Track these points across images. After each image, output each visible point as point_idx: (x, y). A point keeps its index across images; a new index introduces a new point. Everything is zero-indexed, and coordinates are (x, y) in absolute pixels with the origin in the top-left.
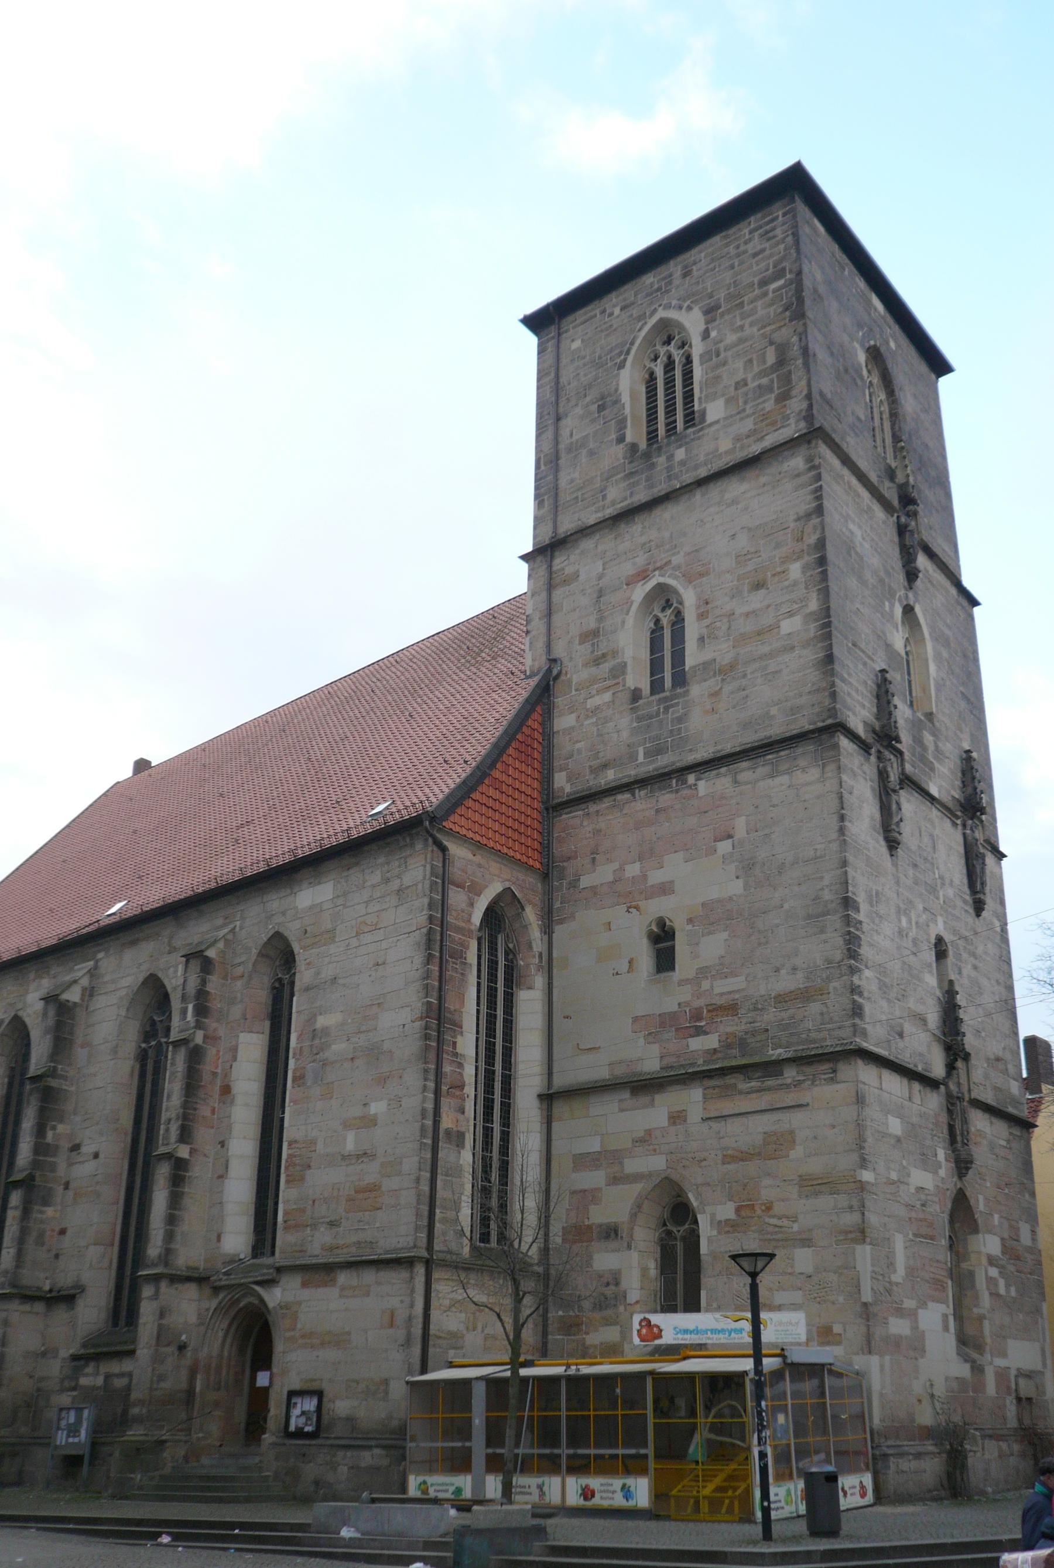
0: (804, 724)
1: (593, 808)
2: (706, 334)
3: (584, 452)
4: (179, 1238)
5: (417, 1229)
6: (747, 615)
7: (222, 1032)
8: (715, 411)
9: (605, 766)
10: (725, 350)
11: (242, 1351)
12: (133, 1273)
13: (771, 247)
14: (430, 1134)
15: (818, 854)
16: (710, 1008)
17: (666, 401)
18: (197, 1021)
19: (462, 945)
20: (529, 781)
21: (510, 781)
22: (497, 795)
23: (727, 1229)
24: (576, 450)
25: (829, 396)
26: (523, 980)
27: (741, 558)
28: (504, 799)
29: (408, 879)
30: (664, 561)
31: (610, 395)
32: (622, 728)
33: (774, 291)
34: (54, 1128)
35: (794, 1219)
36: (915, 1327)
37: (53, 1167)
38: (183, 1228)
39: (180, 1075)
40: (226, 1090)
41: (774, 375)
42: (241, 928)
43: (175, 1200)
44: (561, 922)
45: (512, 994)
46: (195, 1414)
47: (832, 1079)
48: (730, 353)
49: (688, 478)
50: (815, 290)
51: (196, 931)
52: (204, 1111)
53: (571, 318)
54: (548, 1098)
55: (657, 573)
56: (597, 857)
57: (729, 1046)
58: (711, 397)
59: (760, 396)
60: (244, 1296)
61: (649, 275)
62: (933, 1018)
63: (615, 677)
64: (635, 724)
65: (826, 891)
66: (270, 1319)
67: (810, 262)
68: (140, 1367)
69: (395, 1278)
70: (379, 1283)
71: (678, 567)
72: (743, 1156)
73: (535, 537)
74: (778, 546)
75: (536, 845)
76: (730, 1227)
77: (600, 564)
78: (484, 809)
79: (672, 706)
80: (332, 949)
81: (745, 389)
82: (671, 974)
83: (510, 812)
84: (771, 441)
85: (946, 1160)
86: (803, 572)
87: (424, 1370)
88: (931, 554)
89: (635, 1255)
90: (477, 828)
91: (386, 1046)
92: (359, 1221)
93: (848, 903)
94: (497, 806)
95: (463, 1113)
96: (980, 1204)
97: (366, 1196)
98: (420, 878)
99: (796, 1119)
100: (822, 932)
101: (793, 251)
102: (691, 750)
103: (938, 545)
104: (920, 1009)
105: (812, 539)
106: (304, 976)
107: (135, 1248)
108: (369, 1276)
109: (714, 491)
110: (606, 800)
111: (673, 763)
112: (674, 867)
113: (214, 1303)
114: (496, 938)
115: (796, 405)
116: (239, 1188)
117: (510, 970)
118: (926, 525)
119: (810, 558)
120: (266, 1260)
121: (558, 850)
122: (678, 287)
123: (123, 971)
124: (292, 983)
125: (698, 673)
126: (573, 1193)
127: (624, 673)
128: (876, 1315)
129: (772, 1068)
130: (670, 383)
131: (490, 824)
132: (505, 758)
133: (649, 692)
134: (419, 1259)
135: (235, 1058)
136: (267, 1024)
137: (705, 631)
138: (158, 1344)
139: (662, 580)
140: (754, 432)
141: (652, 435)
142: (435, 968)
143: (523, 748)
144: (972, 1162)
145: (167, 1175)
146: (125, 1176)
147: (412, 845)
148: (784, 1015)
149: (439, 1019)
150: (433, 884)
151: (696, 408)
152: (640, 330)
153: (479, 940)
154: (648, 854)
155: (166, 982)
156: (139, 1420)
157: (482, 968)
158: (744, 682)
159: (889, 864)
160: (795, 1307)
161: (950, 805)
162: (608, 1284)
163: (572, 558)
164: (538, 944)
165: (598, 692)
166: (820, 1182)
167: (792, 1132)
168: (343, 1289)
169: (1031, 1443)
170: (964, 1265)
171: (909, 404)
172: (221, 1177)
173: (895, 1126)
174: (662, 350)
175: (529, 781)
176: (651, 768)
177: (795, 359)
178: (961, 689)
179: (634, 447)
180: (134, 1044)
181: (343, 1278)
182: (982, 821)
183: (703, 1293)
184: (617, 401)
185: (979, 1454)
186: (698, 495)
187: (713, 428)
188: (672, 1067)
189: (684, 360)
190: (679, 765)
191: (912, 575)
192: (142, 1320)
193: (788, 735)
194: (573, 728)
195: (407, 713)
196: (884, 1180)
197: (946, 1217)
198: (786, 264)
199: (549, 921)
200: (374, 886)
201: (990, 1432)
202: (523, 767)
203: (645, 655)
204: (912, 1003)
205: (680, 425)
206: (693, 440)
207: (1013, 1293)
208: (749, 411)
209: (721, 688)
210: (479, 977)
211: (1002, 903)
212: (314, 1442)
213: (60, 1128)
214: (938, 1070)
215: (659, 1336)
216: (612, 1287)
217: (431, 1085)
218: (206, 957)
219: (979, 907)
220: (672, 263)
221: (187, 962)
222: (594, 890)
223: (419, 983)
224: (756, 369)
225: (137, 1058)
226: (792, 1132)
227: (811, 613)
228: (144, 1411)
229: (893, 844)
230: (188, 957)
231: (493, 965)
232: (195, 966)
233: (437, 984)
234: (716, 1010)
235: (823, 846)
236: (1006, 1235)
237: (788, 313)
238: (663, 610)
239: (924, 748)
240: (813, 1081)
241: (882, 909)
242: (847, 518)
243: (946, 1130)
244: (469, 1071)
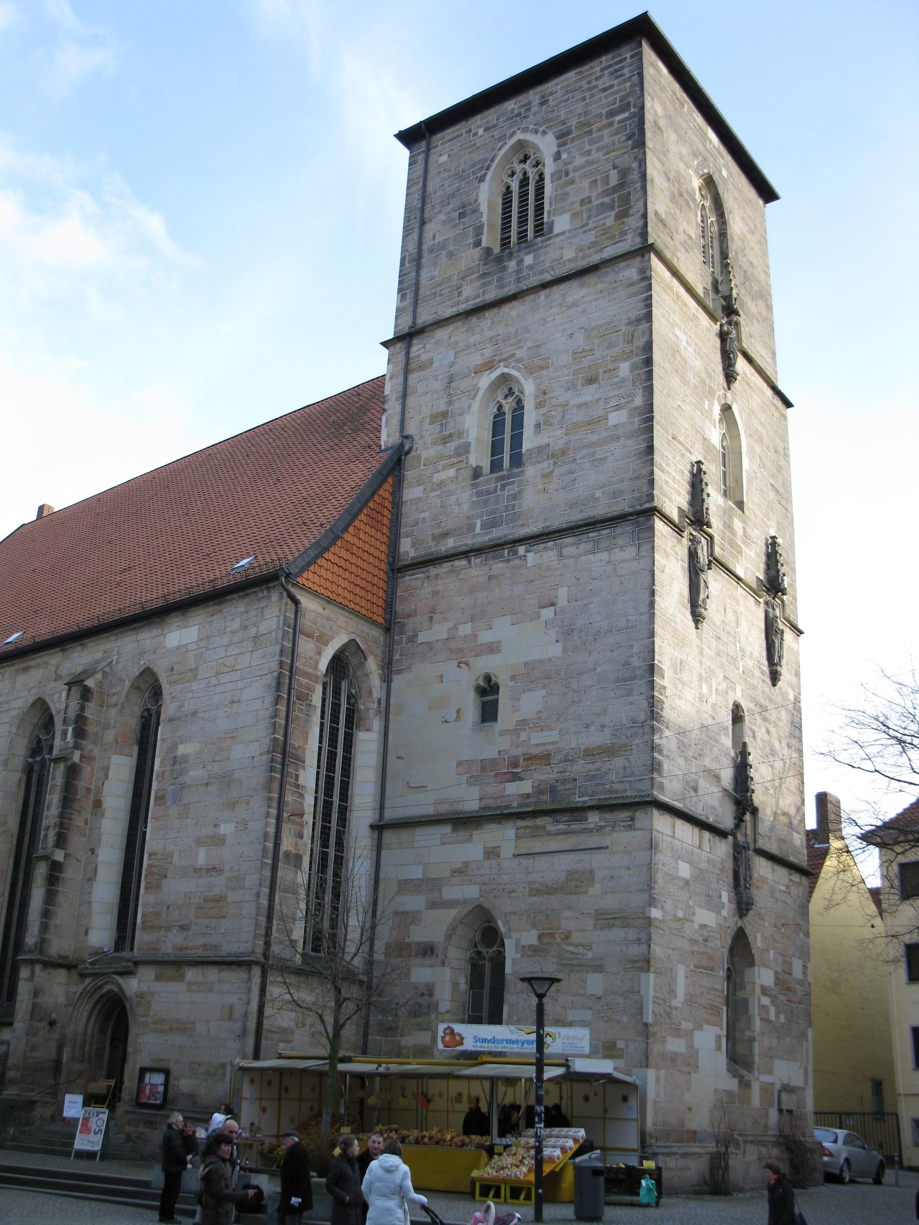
0: (623, 506)
1: (433, 571)
2: (557, 157)
3: (444, 253)
4: (52, 930)
5: (256, 937)
6: (579, 406)
7: (96, 753)
8: (561, 223)
9: (446, 535)
10: (574, 171)
11: (103, 1031)
12: (14, 957)
13: (619, 84)
14: (270, 854)
15: (630, 625)
16: (526, 757)
17: (520, 212)
18: (75, 742)
19: (308, 689)
20: (378, 545)
21: (361, 544)
23: (530, 953)
24: (438, 251)
25: (664, 216)
26: (362, 722)
27: (578, 355)
29: (263, 628)
30: (509, 354)
31: (470, 204)
32: (462, 502)
33: (619, 122)
35: (589, 947)
36: (690, 1046)
38: (56, 921)
39: (58, 789)
40: (98, 804)
41: (615, 195)
42: (117, 663)
43: (51, 896)
44: (399, 672)
45: (352, 734)
47: (630, 826)
48: (577, 174)
49: (534, 281)
50: (656, 123)
51: (79, 659)
52: (78, 821)
53: (440, 135)
54: (379, 828)
55: (502, 364)
56: (435, 616)
57: (541, 792)
58: (560, 211)
59: (602, 213)
60: (107, 983)
61: (510, 102)
62: (727, 775)
63: (459, 455)
64: (475, 499)
65: (635, 658)
66: (128, 1006)
67: (653, 100)
69: (236, 977)
70: (220, 982)
72: (549, 890)
73: (396, 326)
75: (381, 603)
76: (533, 951)
77: (451, 354)
78: (336, 569)
79: (509, 484)
80: (195, 686)
81: (589, 206)
82: (493, 724)
83: (359, 572)
84: (610, 253)
85: (729, 901)
86: (631, 371)
87: (256, 1057)
89: (447, 971)
90: (329, 585)
91: (237, 775)
92: (207, 927)
94: (348, 566)
95: (302, 838)
96: (757, 941)
97: (213, 904)
98: (275, 627)
99: (597, 860)
100: (629, 694)
101: (637, 89)
102: (523, 525)
104: (714, 766)
105: (641, 342)
106: (169, 708)
107: (16, 935)
108: (212, 973)
109: (557, 291)
110: (445, 565)
111: (506, 536)
112: (501, 629)
113: (81, 988)
114: (340, 684)
115: (633, 222)
117: (351, 713)
118: (750, 334)
119: (639, 359)
120: (125, 954)
121: (400, 608)
122: (535, 114)
124: (159, 714)
125: (533, 455)
126: (396, 913)
127: (468, 452)
128: (655, 1034)
129: (577, 812)
130: (524, 196)
131: (341, 582)
132: (357, 523)
133: (489, 470)
134: (257, 963)
135: (106, 777)
136: (136, 749)
137: (542, 418)
138: (32, 1018)
139: (506, 370)
141: (505, 242)
142: (282, 708)
143: (374, 515)
144: (752, 904)
145: (45, 874)
147: (269, 597)
148: (591, 767)
149: (284, 754)
150: (285, 633)
151: (545, 220)
152: (500, 149)
153: (325, 686)
154: (478, 616)
155: (51, 706)
156: (12, 1082)
157: (326, 710)
158: (574, 466)
159: (694, 637)
160: (583, 1024)
161: (754, 585)
162: (423, 995)
164: (378, 691)
165: (444, 468)
166: (613, 916)
167: (592, 871)
168: (189, 984)
169: (789, 1149)
170: (740, 994)
172: (90, 879)
173: (684, 870)
174: (518, 168)
175: (378, 545)
176: (486, 538)
177: (634, 183)
178: (771, 481)
179: (488, 251)
180: (22, 758)
181: (191, 974)
182: (783, 601)
183: (506, 1008)
184: (475, 211)
185: (740, 1156)
187: (559, 239)
188: (489, 808)
189: (537, 178)
191: (730, 377)
192: (19, 997)
193: (609, 515)
194: (419, 499)
195: (275, 477)
196: (671, 917)
197: (726, 951)
198: (631, 99)
199: (388, 670)
200: (233, 632)
201: (751, 1138)
202: (373, 532)
203: (487, 437)
204: (707, 762)
205: (530, 234)
206: (541, 248)
207: (782, 1019)
208: (591, 226)
209: (553, 471)
210: (322, 717)
212: (159, 1113)
214: (727, 822)
215: (461, 1044)
216: (426, 997)
217: (274, 812)
218: (86, 686)
219: (775, 677)
220: (531, 92)
221: (69, 690)
222: (429, 644)
223: (267, 721)
224: (600, 189)
225: (24, 771)
226: (592, 871)
227: (636, 408)
228: (19, 1074)
229: (697, 617)
230: (70, 684)
231: (336, 708)
232: (76, 691)
233: (283, 722)
235: (634, 618)
236: (779, 969)
237: (630, 142)
238: (506, 397)
239: (733, 533)
240: (613, 827)
241: (685, 677)
242: (673, 325)
243: (731, 876)
244: (309, 801)
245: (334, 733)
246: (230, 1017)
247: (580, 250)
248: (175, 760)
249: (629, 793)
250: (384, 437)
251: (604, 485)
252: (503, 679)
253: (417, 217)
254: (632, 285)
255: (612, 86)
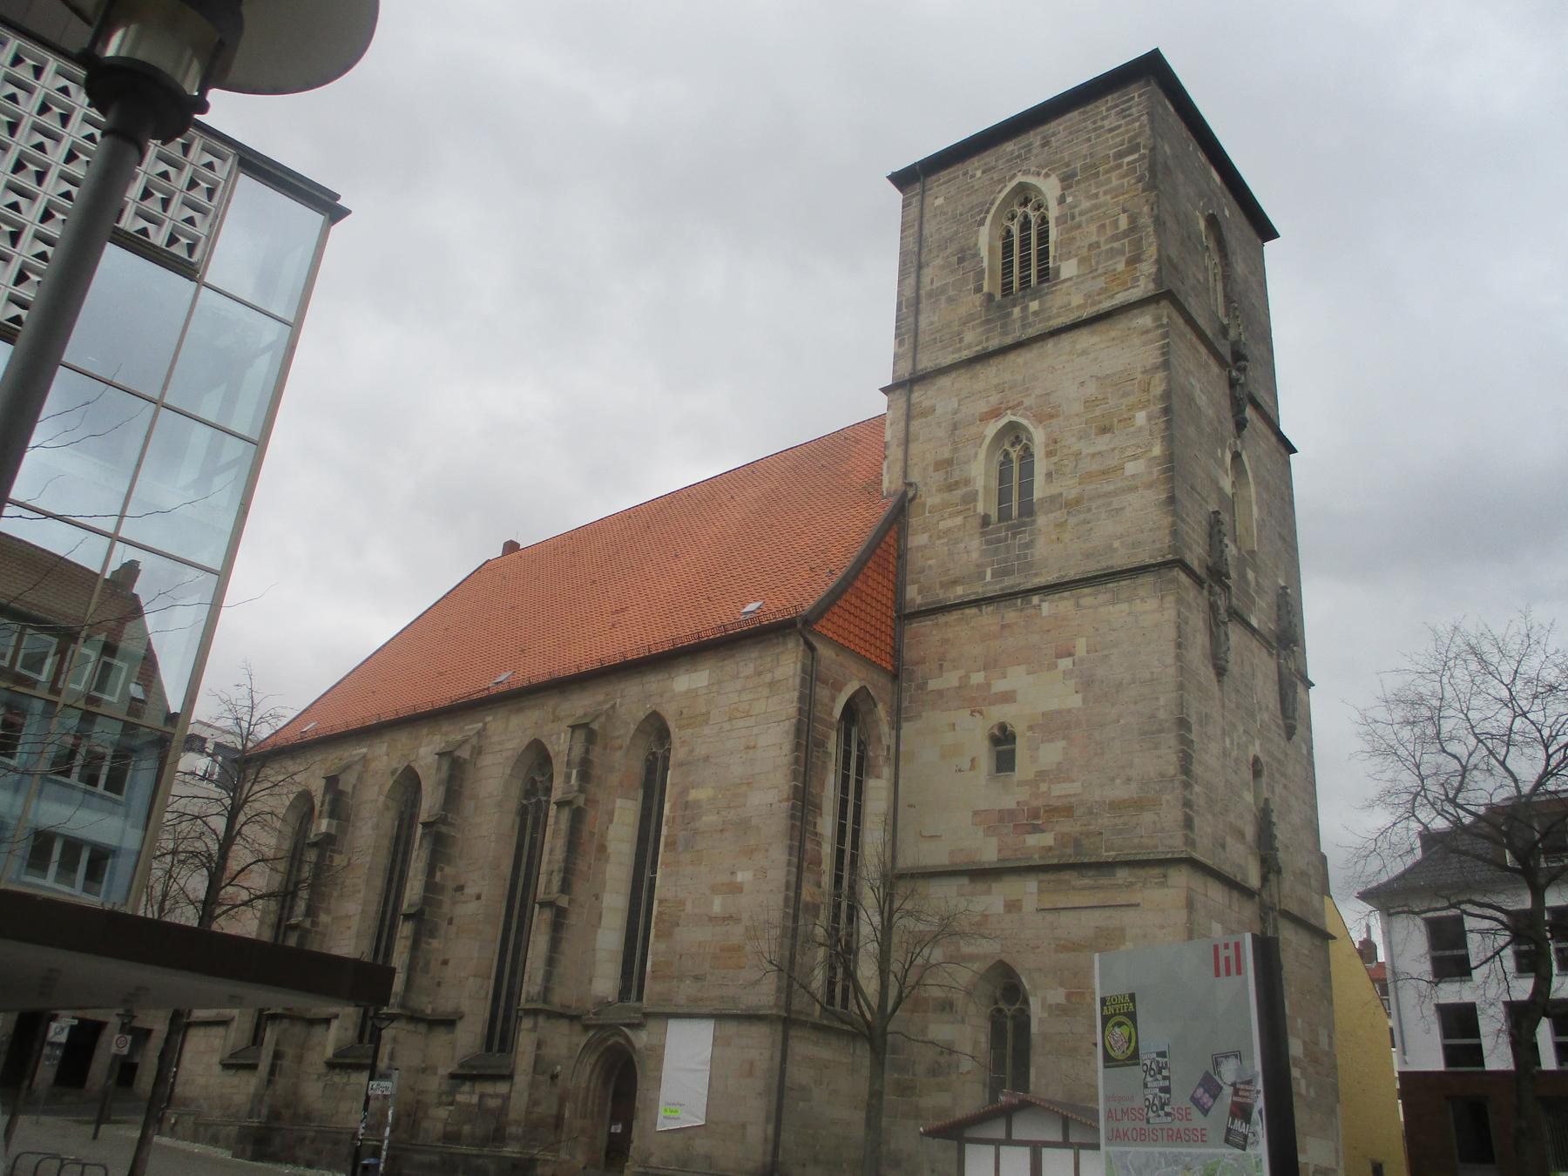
1: (942, 619)
3: (943, 298)
6: (1093, 455)
8: (1068, 269)
9: (955, 582)
13: (1127, 124)
22: (857, 602)
27: (1090, 403)
28: (863, 606)
29: (779, 673)
32: (972, 548)
34: (442, 870)
37: (439, 904)
40: (602, 848)
44: (908, 719)
46: (564, 1137)
51: (580, 705)
53: (934, 178)
62: (1250, 831)
66: (635, 1058)
68: (519, 1094)
71: (1029, 408)
74: (1125, 395)
76: (1060, 1011)
77: (955, 400)
80: (706, 730)
88: (1257, 406)
93: (1183, 723)
94: (858, 613)
99: (1128, 917)
100: (1156, 748)
103: (1262, 396)
106: (678, 753)
109: (1066, 341)
112: (1016, 679)
113: (583, 1040)
116: (609, 938)
117: (860, 760)
123: (508, 735)
124: (666, 759)
127: (975, 500)
129: (1105, 867)
130: (1025, 242)
135: (611, 821)
136: (641, 793)
138: (535, 1071)
139: (1014, 418)
140: (1103, 291)
141: (1007, 288)
146: (502, 919)
155: (549, 748)
158: (1089, 516)
163: (930, 393)
165: (951, 516)
171: (1240, 268)
174: (1019, 211)
183: (1033, 1071)
184: (976, 255)
186: (1050, 345)
190: (1022, 587)
191: (1240, 425)
194: (925, 547)
204: (1232, 818)
211: (1309, 728)
213: (448, 870)
214: (1254, 881)
217: (795, 860)
222: (940, 693)
224: (1109, 233)
226: (1122, 929)
229: (1221, 671)
230: (574, 728)
231: (847, 755)
232: (581, 735)
234: (1052, 810)
238: (1013, 445)
245: (846, 779)
246: (751, 1073)
247: (1088, 296)
248: (687, 805)
249: (1160, 849)
250: (885, 484)
251: (1122, 536)
252: (1019, 728)
253: (913, 262)
254: (1147, 332)
255: (1119, 127)
